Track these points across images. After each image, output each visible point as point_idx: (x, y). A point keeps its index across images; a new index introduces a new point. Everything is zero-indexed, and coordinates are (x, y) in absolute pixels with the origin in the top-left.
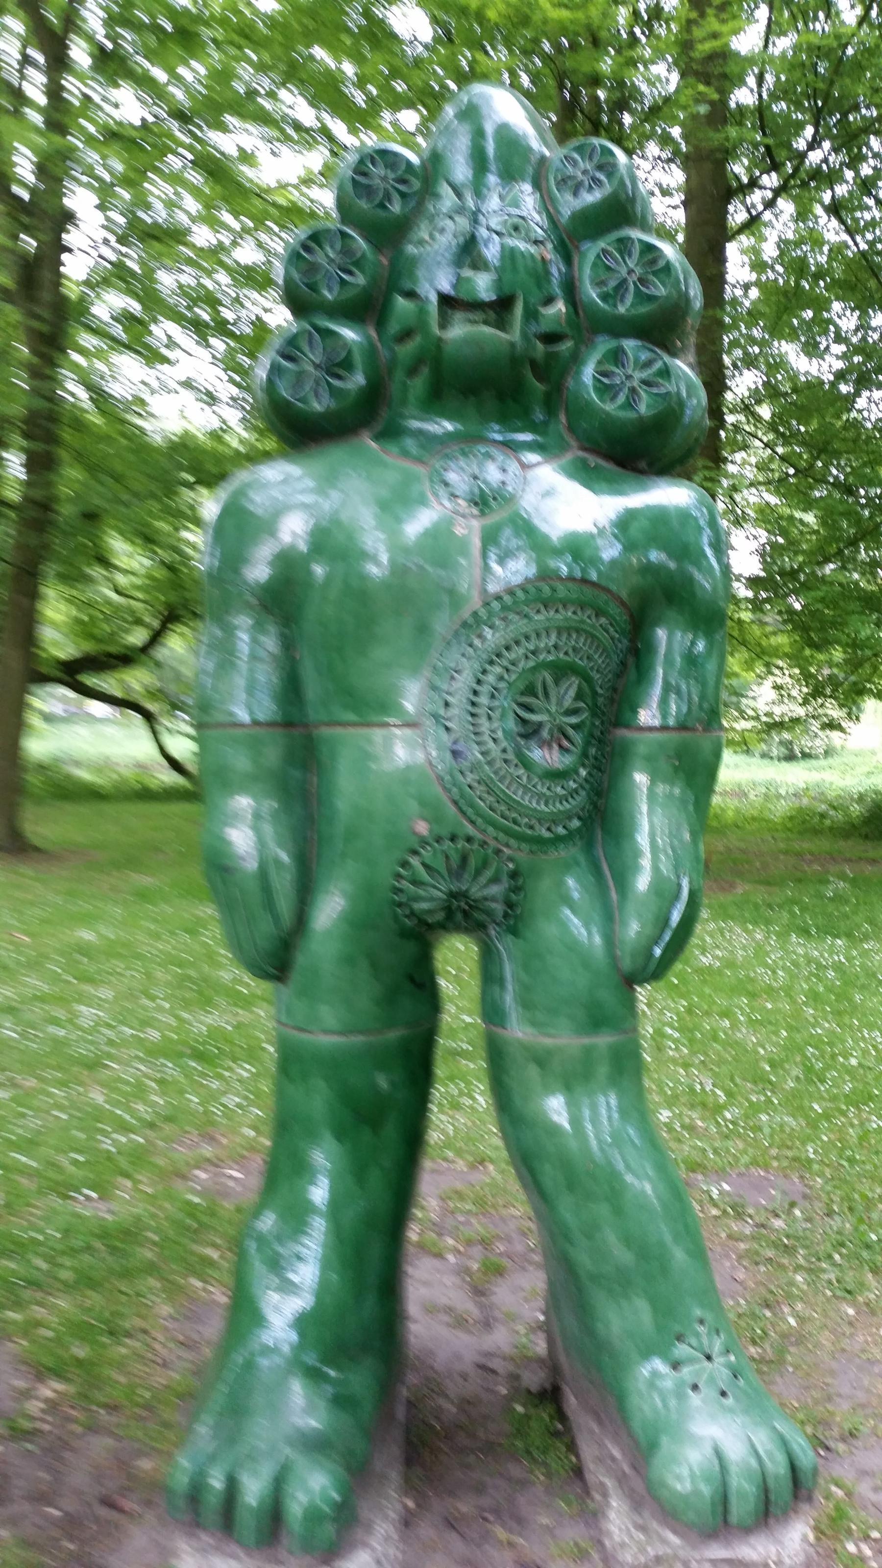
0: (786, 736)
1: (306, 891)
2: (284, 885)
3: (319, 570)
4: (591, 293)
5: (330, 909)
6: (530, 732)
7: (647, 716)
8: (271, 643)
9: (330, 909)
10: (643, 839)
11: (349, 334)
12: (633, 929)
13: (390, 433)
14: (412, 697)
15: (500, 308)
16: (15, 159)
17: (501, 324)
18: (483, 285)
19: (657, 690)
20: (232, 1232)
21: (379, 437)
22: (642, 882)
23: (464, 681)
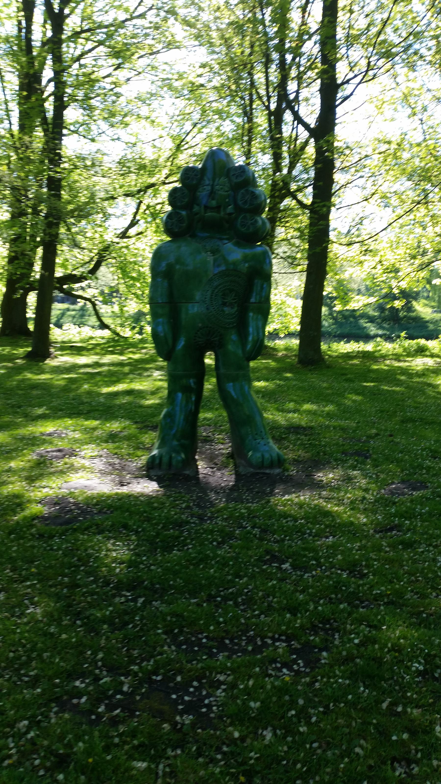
0: (428, 187)
1: (175, 340)
2: (170, 341)
3: (178, 267)
4: (240, 203)
5: (181, 343)
6: (224, 304)
7: (253, 300)
8: (166, 283)
9: (181, 343)
10: (251, 330)
11: (184, 213)
12: (249, 346)
13: (193, 236)
14: (198, 296)
15: (218, 208)
16: (153, 345)
17: (219, 212)
18: (214, 203)
19: (254, 294)
20: (406, 92)
21: (190, 236)
22: (250, 338)
23: (209, 293)
